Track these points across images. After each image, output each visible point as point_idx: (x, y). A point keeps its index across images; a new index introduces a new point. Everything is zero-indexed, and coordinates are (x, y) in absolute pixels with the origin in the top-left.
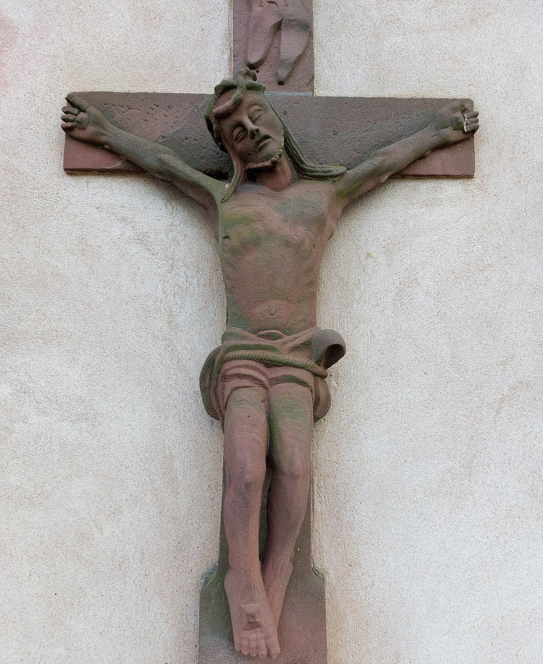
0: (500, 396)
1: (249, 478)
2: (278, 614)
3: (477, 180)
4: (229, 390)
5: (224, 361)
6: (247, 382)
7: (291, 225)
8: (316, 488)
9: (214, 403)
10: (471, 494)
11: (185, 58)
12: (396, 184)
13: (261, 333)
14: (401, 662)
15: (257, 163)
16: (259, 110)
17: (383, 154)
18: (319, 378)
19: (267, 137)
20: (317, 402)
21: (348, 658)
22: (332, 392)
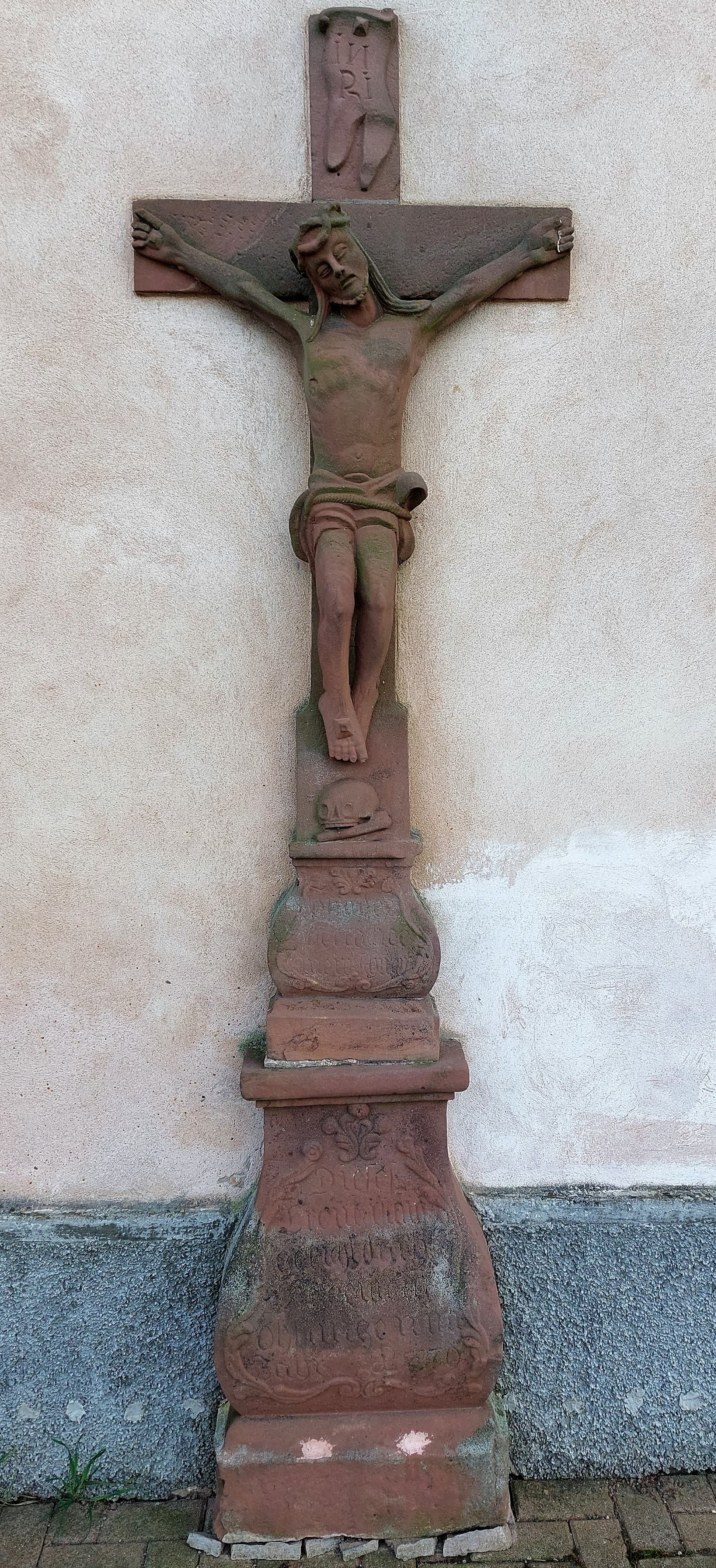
0: (581, 537)
1: (340, 609)
2: (366, 731)
3: (572, 304)
4: (319, 532)
5: (313, 504)
6: (335, 524)
7: (376, 369)
8: (400, 629)
9: (303, 545)
10: (548, 632)
11: (257, 152)
12: (486, 307)
13: (347, 476)
15: (342, 299)
16: (344, 248)
17: (471, 281)
18: (403, 521)
19: (352, 276)
20: (401, 544)
22: (416, 534)
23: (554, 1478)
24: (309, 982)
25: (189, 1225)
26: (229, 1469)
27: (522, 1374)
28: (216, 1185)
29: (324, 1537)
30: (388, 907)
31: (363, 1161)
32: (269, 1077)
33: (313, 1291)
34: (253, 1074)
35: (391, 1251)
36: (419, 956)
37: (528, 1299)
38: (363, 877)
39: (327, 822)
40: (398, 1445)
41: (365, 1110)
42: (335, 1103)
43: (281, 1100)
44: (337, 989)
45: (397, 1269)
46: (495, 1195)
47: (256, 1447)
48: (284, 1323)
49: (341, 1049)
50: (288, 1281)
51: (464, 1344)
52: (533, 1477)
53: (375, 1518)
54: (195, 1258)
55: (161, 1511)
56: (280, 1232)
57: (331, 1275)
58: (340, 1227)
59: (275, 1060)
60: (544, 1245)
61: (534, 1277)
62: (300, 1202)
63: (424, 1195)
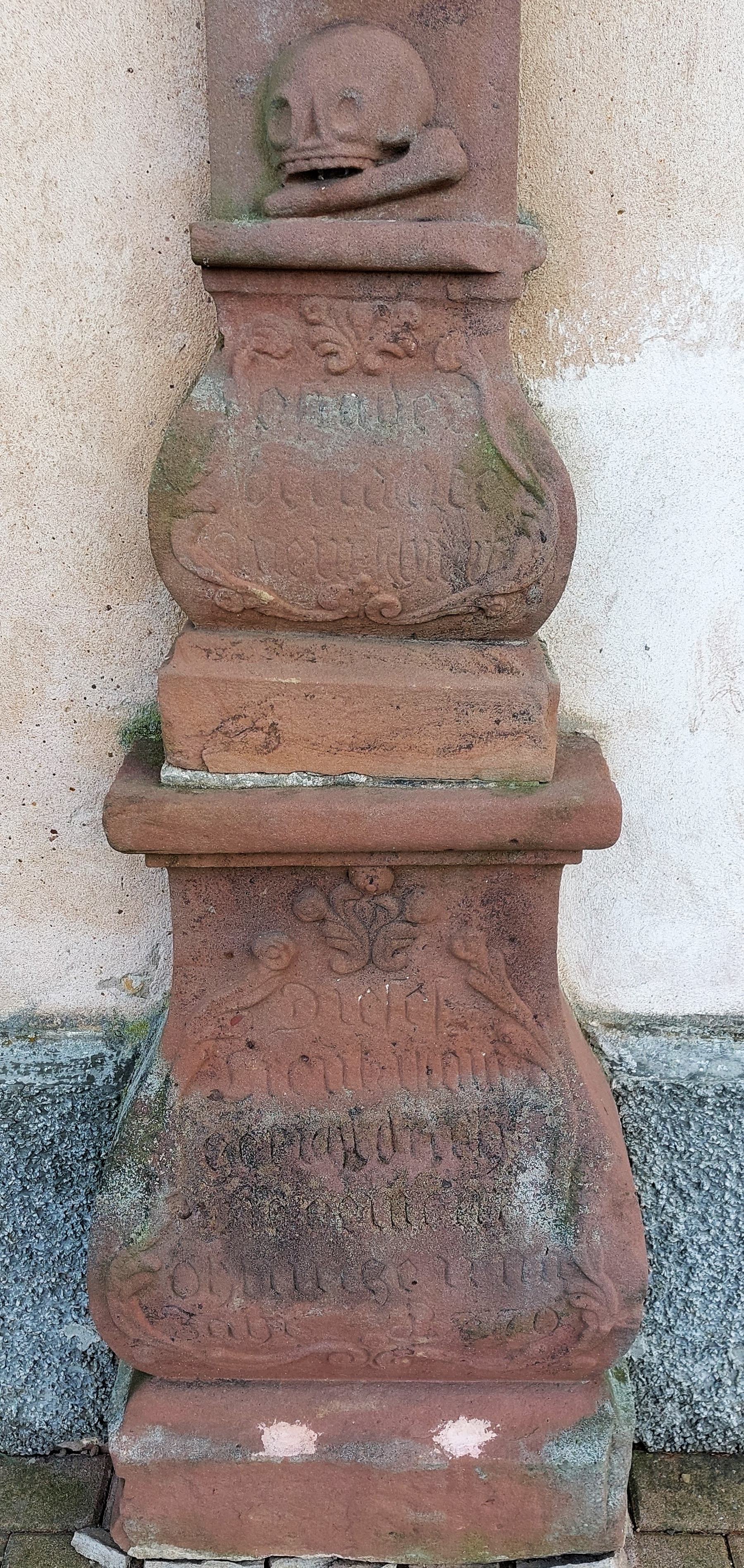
14: (698, 68)
21: (571, 57)
23: (700, 1450)
24: (254, 595)
25: (46, 1060)
26: (131, 1465)
27: (662, 1309)
28: (95, 994)
29: (302, 1557)
30: (449, 410)
31: (378, 972)
32: (168, 807)
33: (276, 1207)
34: (131, 800)
35: (432, 1140)
36: (524, 539)
37: (686, 1199)
38: (386, 327)
39: (290, 155)
40: (435, 1439)
41: (384, 879)
42: (320, 863)
43: (200, 856)
44: (321, 615)
45: (443, 1175)
46: (641, 1029)
47: (178, 1429)
48: (220, 1257)
49: (335, 749)
50: (227, 1187)
51: (569, 1303)
52: (664, 1449)
53: (391, 1537)
54: (62, 1116)
55: (37, 1475)
56: (211, 1097)
57: (312, 1181)
58: (331, 1092)
59: (184, 769)
60: (729, 1117)
61: (702, 1166)
62: (251, 1045)
63: (502, 1039)
